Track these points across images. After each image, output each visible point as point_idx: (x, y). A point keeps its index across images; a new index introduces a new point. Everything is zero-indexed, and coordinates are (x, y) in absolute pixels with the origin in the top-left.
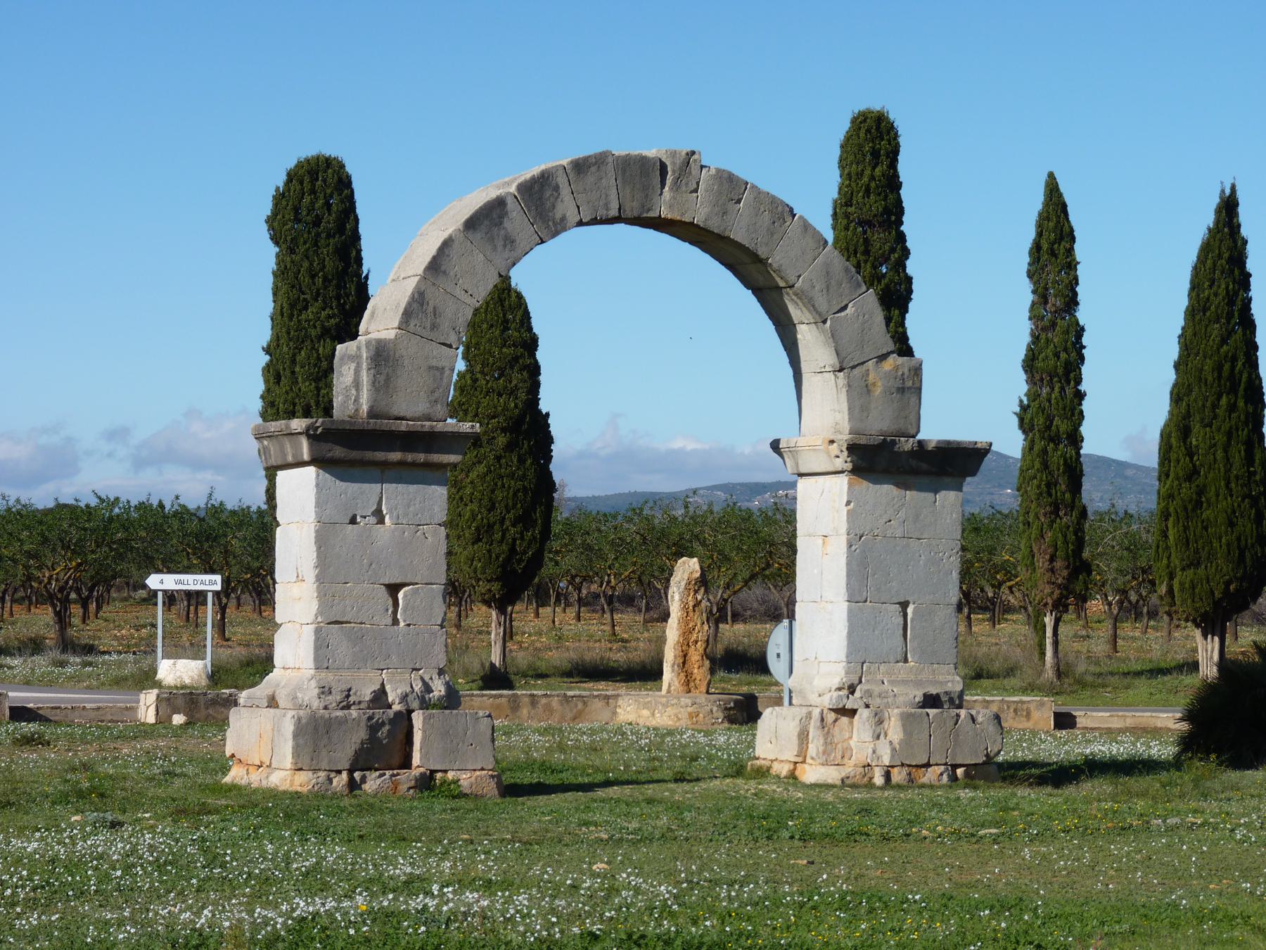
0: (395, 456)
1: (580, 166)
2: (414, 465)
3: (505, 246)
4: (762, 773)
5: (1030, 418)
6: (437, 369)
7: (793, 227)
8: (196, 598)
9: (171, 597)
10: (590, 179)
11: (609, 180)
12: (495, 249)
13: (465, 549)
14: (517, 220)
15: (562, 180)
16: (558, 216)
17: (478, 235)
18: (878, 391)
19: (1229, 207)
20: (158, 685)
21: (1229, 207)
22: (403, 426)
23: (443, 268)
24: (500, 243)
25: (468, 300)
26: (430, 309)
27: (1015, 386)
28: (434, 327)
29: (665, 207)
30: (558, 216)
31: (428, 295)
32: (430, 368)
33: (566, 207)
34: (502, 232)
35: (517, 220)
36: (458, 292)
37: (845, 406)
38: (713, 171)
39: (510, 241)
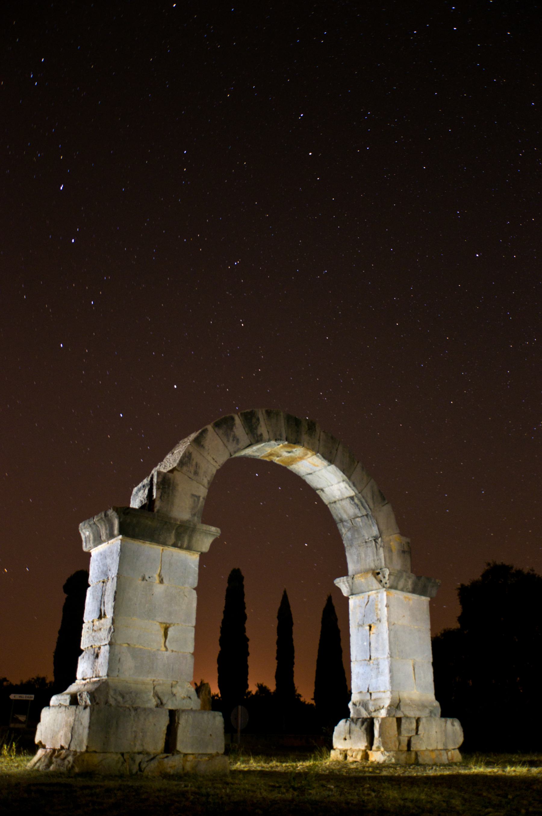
3: (233, 440)
4: (506, 772)
6: (196, 496)
12: (228, 441)
13: (11, 756)
16: (259, 433)
17: (221, 432)
19: (285, 597)
21: (285, 597)
23: (202, 443)
24: (231, 439)
25: (215, 464)
26: (194, 463)
30: (259, 433)
31: (193, 455)
32: (193, 495)
34: (232, 433)
36: (210, 458)
37: (193, 662)
38: (9, 683)
39: (236, 440)
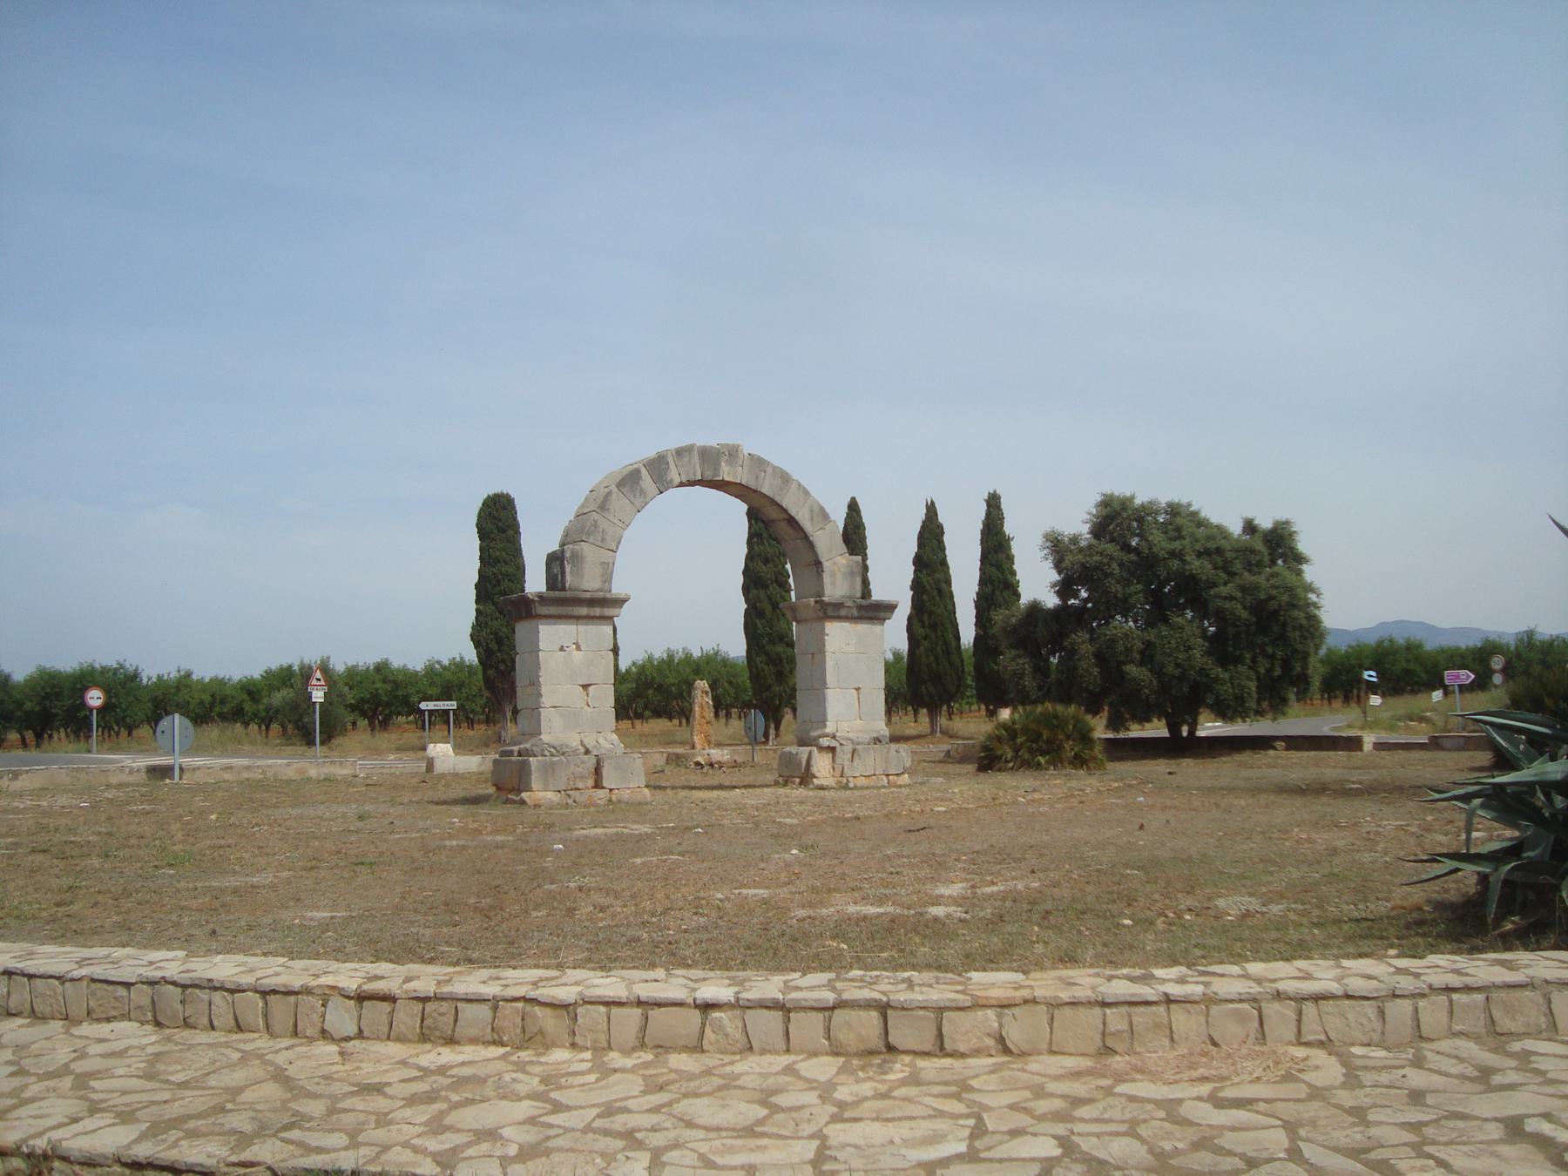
0: (584, 611)
1: (680, 452)
2: (594, 618)
5: (917, 586)
7: (794, 487)
8: (446, 712)
9: (430, 711)
10: (686, 459)
11: (696, 459)
14: (647, 481)
15: (670, 459)
18: (839, 576)
20: (72, 1073)
22: (588, 595)
27: (737, 606)
28: (603, 540)
29: (726, 474)
33: (674, 475)
35: (647, 481)
39: (643, 493)
